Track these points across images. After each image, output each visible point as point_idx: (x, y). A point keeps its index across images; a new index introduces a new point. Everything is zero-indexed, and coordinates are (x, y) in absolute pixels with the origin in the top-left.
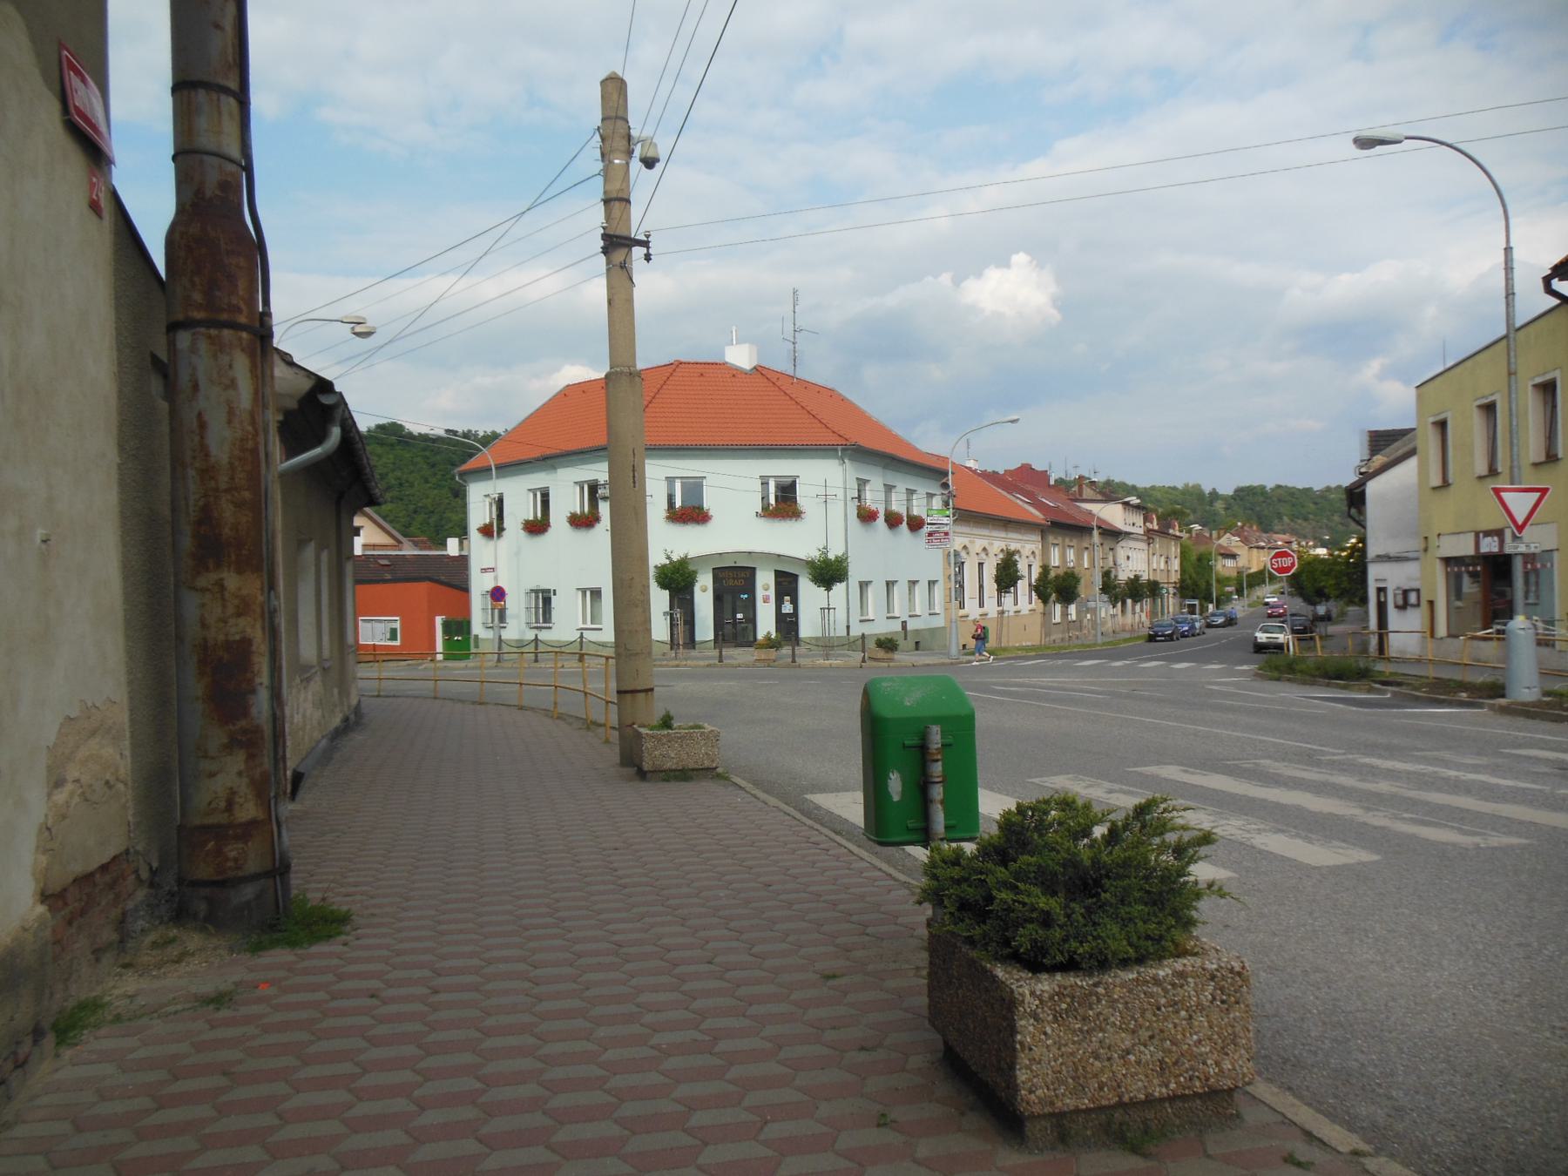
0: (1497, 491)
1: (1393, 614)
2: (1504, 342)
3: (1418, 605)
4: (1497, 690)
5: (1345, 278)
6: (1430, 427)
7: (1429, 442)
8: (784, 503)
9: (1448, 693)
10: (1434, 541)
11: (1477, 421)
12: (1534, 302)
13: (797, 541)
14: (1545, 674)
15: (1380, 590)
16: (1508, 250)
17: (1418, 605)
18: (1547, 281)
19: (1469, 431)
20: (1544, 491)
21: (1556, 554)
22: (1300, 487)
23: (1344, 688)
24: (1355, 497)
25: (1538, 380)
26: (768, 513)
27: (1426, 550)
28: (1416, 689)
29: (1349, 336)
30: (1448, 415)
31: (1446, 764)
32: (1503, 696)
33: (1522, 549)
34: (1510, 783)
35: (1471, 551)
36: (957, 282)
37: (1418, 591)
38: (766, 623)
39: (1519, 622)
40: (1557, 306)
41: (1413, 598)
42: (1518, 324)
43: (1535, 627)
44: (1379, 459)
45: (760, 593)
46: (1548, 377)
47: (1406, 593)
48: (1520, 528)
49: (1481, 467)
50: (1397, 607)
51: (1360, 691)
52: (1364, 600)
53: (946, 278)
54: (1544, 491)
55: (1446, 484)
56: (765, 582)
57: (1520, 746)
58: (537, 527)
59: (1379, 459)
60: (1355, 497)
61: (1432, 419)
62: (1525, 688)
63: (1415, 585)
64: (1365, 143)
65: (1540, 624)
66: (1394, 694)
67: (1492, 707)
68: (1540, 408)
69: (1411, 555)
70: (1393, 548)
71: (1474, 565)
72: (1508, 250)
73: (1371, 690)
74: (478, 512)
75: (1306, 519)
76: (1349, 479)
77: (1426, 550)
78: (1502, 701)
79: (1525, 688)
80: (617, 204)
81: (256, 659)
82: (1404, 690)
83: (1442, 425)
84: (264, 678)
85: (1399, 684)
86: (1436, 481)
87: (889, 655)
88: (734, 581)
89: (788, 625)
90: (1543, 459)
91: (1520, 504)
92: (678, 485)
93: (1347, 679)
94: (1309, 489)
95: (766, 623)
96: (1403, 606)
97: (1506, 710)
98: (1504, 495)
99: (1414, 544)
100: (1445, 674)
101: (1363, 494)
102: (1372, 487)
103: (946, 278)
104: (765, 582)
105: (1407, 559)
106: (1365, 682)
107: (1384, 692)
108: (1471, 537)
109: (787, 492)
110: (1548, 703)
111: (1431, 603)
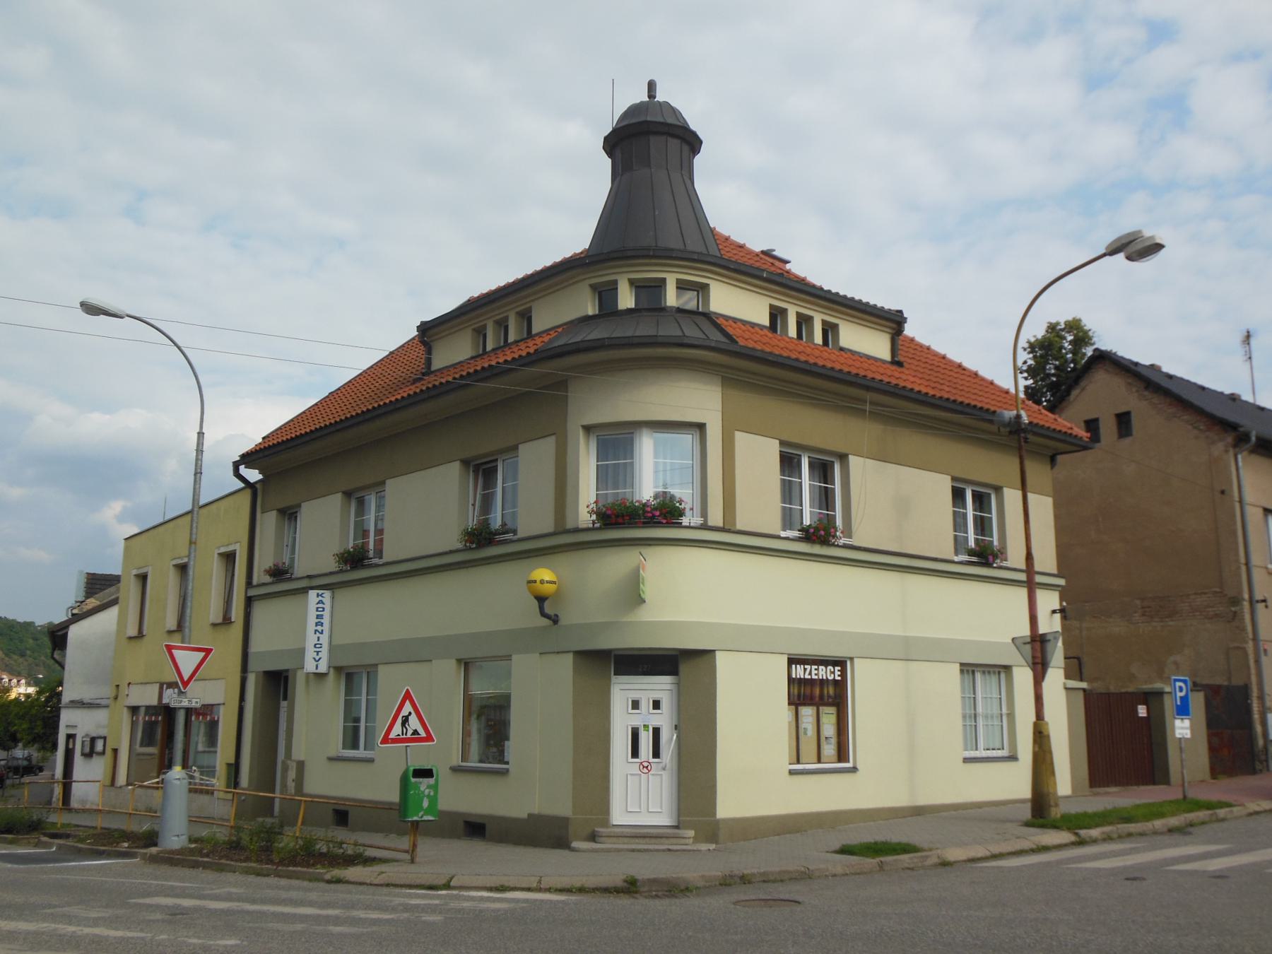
0: (169, 648)
1: (78, 759)
2: (188, 518)
3: (103, 753)
4: (151, 839)
5: (96, 416)
6: (133, 579)
7: (130, 590)
9: (111, 844)
10: (124, 690)
11: (172, 578)
12: (221, 481)
14: (193, 820)
15: (70, 737)
16: (201, 434)
17: (103, 753)
18: (236, 466)
19: (165, 586)
20: (208, 651)
21: (222, 708)
22: (21, 620)
23: (11, 842)
24: (57, 637)
25: (223, 550)
27: (116, 698)
28: (82, 841)
29: (94, 472)
30: (150, 570)
31: (69, 919)
32: (156, 845)
33: (185, 703)
34: (119, 934)
35: (155, 702)
37: (105, 738)
39: (177, 772)
41: (99, 746)
42: (202, 502)
43: (192, 777)
44: (92, 602)
46: (231, 548)
47: (93, 740)
48: (186, 684)
49: (171, 623)
50: (83, 754)
51: (28, 844)
52: (55, 747)
54: (208, 651)
55: (140, 635)
57: (149, 895)
59: (92, 602)
60: (57, 637)
61: (135, 572)
62: (175, 837)
63: (103, 732)
64: (91, 309)
65: (197, 774)
66: (60, 847)
67: (144, 856)
68: (223, 574)
69: (103, 702)
70: (87, 694)
71: (157, 715)
72: (201, 434)
73: (36, 846)
75: (23, 655)
76: (59, 617)
77: (116, 698)
78: (154, 850)
79: (175, 837)
81: (80, 933)
82: (70, 842)
83: (143, 578)
84: (651, 847)
85: (67, 836)
86: (133, 631)
87: (475, 716)
90: (220, 620)
91: (187, 661)
93: (18, 833)
94: (31, 624)
96: (89, 754)
97: (154, 859)
98: (176, 652)
99: (108, 691)
100: (115, 824)
101: (65, 636)
102: (74, 632)
105: (98, 706)
106: (35, 835)
107: (50, 845)
108: (156, 688)
110: (191, 850)
111: (115, 751)
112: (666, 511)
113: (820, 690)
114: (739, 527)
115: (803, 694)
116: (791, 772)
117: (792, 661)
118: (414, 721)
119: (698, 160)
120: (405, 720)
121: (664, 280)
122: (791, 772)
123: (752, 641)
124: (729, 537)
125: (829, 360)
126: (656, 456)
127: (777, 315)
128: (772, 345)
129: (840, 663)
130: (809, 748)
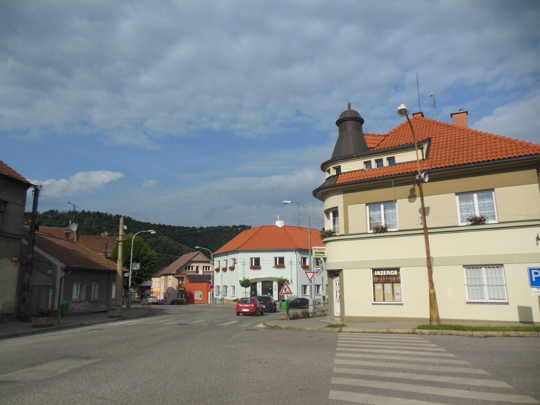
8: (280, 263)
26: (277, 266)
56: (275, 285)
58: (225, 270)
88: (267, 284)
92: (395, 273)
104: (275, 285)
109: (282, 260)
112: (330, 234)
113: (386, 277)
114: (350, 233)
115: (378, 280)
116: (373, 304)
117: (374, 270)
118: (287, 289)
119: (363, 125)
120: (286, 289)
121: (382, 159)
122: (373, 304)
123: (357, 265)
124: (348, 236)
125: (394, 171)
126: (479, 201)
127: (368, 164)
128: (381, 173)
129: (398, 269)
130: (379, 297)
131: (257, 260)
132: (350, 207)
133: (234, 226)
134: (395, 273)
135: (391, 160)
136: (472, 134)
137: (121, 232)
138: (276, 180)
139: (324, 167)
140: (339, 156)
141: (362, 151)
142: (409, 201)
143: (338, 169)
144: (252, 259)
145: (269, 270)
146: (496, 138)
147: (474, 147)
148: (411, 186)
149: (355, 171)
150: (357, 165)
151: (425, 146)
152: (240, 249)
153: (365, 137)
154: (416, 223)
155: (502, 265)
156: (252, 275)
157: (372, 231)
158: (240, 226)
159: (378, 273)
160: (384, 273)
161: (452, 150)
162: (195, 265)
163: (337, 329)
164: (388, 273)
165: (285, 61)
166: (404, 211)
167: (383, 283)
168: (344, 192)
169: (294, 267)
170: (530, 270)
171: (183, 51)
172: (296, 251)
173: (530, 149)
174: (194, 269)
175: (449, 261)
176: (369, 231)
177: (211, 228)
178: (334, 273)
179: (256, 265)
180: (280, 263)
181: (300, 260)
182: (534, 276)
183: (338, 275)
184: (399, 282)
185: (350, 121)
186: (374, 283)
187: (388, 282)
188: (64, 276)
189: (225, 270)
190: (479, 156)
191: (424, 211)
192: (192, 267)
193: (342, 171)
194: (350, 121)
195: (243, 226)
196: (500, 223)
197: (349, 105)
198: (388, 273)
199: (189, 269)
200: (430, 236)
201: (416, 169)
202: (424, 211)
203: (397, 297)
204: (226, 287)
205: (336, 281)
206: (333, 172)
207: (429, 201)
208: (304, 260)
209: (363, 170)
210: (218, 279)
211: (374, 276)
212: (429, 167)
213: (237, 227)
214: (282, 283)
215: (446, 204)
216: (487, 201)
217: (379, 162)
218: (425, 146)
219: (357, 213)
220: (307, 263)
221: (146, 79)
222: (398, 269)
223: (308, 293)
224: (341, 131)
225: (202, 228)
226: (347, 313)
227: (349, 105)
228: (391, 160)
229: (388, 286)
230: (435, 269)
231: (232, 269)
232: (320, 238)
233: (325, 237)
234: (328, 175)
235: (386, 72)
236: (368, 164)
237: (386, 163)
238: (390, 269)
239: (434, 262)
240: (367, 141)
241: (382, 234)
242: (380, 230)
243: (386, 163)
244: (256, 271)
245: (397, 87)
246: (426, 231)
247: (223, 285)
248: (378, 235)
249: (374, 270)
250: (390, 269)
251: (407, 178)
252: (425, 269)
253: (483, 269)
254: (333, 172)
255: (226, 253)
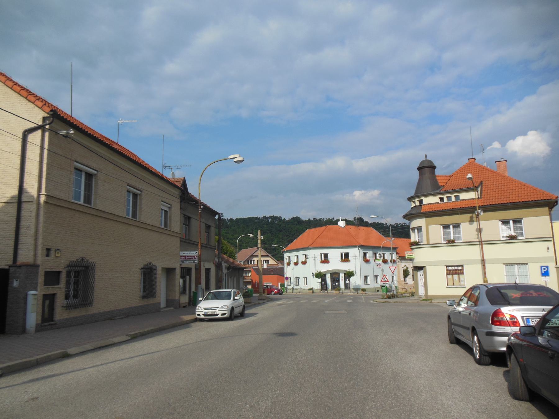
8: (346, 258)
13: (346, 267)
26: (343, 261)
36: (503, 144)
38: (342, 285)
40: (515, 355)
45: (341, 278)
53: (496, 145)
56: (342, 276)
58: (296, 264)
74: (286, 261)
80: (427, 170)
88: (335, 276)
89: (347, 286)
92: (461, 268)
95: (342, 285)
103: (496, 145)
104: (342, 276)
109: (347, 255)
113: (455, 271)
114: (431, 243)
115: (449, 272)
117: (447, 266)
124: (429, 245)
127: (442, 199)
129: (462, 266)
130: (451, 283)
131: (326, 256)
132: (430, 227)
133: (264, 217)
134: (461, 268)
135: (457, 197)
136: (510, 180)
137: (259, 241)
138: (305, 168)
139: (410, 199)
140: (420, 193)
141: (436, 188)
142: (470, 224)
143: (421, 202)
144: (321, 254)
145: (335, 263)
146: (524, 185)
147: (511, 191)
148: (471, 215)
149: (433, 204)
150: (435, 199)
151: (479, 189)
152: (311, 247)
153: (437, 178)
154: (474, 237)
155: (527, 264)
156: (324, 268)
157: (445, 242)
158: (271, 217)
159: (449, 268)
160: (453, 268)
161: (497, 192)
162: (256, 259)
163: (429, 301)
164: (456, 268)
165: (314, 44)
166: (467, 230)
167: (453, 274)
168: (426, 217)
169: (358, 261)
170: (541, 267)
171: (208, 37)
172: (359, 247)
173: (544, 195)
174: (256, 263)
175: (495, 261)
176: (443, 242)
177: (240, 219)
178: (421, 268)
179: (325, 259)
180: (346, 258)
181: (362, 255)
182: (543, 270)
183: (422, 269)
184: (463, 273)
185: (427, 168)
186: (447, 274)
187: (456, 274)
188: (227, 273)
189: (296, 264)
190: (514, 199)
191: (480, 230)
192: (254, 261)
193: (424, 203)
194: (427, 168)
195: (273, 216)
196: (526, 239)
197: (426, 156)
198: (456, 268)
199: (251, 263)
200: (484, 246)
201: (474, 205)
202: (480, 230)
203: (462, 283)
204: (298, 279)
205: (420, 273)
206: (418, 203)
207: (483, 224)
208: (365, 254)
209: (438, 203)
210: (289, 271)
211: (447, 270)
212: (483, 204)
213: (267, 218)
214: (349, 275)
215: (494, 227)
216: (518, 225)
217: (449, 198)
218: (479, 189)
219: (434, 230)
220: (368, 258)
221: (172, 67)
222: (462, 266)
223: (369, 282)
224: (421, 174)
225: (231, 219)
226: (430, 293)
227: (426, 156)
228: (457, 197)
229: (456, 276)
230: (487, 266)
231: (304, 263)
232: (409, 246)
233: (413, 245)
234: (413, 205)
235: (421, 53)
236: (442, 199)
237: (453, 199)
238: (457, 266)
239: (486, 262)
240: (439, 181)
241: (452, 244)
242: (451, 242)
243: (453, 199)
244: (325, 265)
245: (433, 67)
246: (481, 243)
247: (295, 276)
248: (449, 244)
249: (447, 266)
250: (457, 266)
251: (468, 210)
252: (480, 267)
253: (516, 266)
254: (418, 203)
255: (298, 250)
